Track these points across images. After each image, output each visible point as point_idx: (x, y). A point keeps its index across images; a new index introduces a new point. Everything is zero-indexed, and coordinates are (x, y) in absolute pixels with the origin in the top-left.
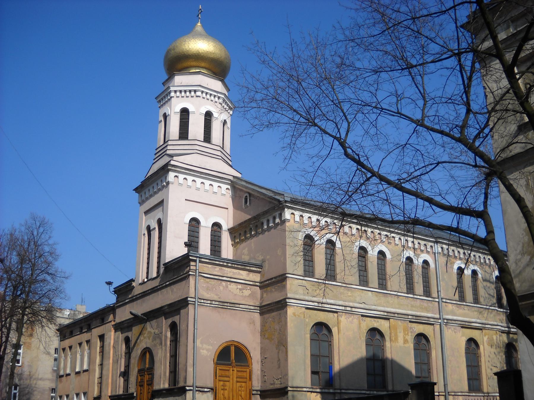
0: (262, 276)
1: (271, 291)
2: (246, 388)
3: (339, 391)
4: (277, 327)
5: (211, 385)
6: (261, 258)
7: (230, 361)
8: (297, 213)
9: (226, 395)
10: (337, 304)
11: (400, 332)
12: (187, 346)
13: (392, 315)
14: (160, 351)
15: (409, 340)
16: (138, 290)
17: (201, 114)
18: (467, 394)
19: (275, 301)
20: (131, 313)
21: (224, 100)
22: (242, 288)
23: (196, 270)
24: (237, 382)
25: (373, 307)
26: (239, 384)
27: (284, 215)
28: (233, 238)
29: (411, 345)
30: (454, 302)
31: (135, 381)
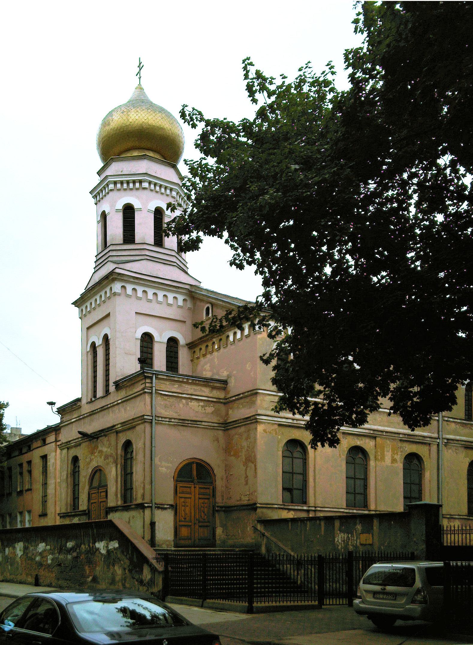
1: (238, 408)
3: (313, 509)
5: (172, 502)
9: (187, 512)
15: (398, 460)
16: (86, 409)
17: (149, 211)
18: (466, 517)
23: (152, 387)
24: (200, 498)
29: (400, 465)
30: (459, 421)
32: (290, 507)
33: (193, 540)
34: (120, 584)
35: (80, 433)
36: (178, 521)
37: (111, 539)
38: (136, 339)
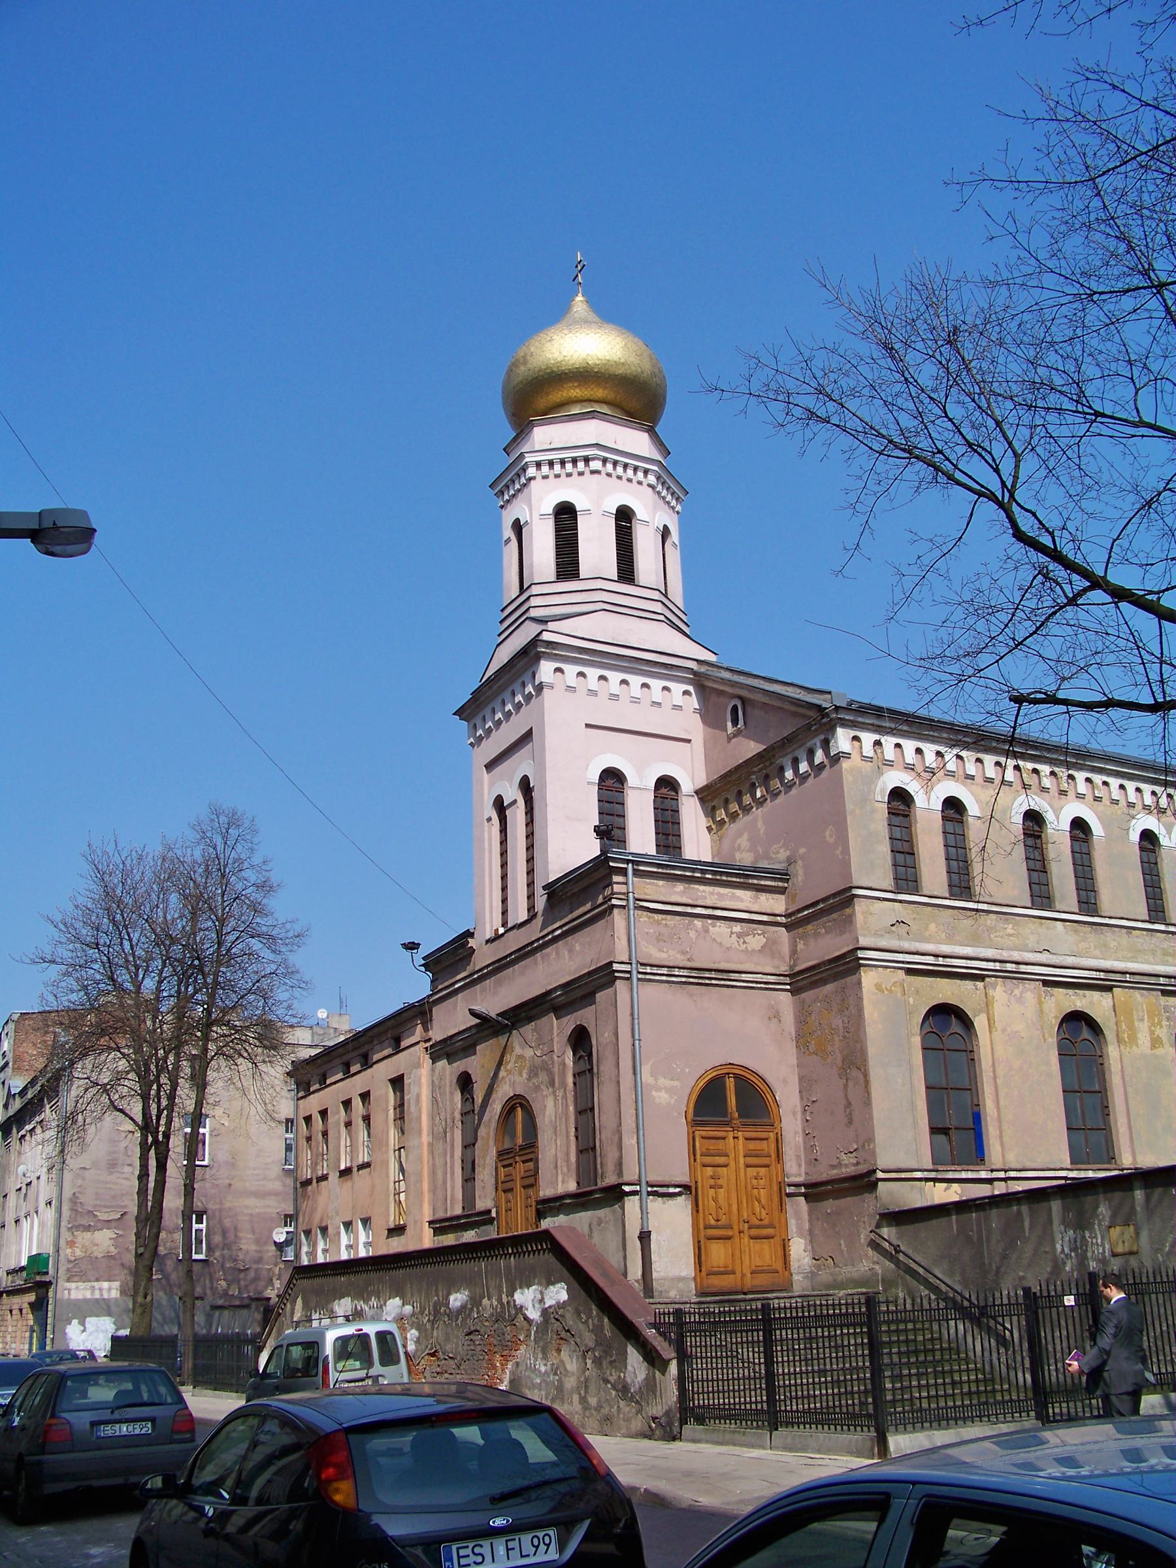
0: (791, 899)
1: (817, 935)
2: (771, 1180)
4: (838, 1022)
5: (685, 1179)
6: (783, 854)
7: (726, 1116)
8: (868, 738)
10: (981, 955)
11: (1142, 1020)
12: (618, 1082)
13: (1118, 977)
14: (550, 1103)
15: (1165, 1039)
16: (483, 957)
17: (606, 513)
19: (827, 958)
20: (473, 1013)
21: (658, 478)
22: (740, 933)
24: (747, 1166)
25: (1070, 961)
26: (752, 1171)
27: (836, 742)
28: (710, 812)
31: (493, 1180)
32: (950, 1175)
33: (739, 1274)
34: (576, 1397)
36: (702, 1226)
37: (550, 1282)
38: (589, 783)
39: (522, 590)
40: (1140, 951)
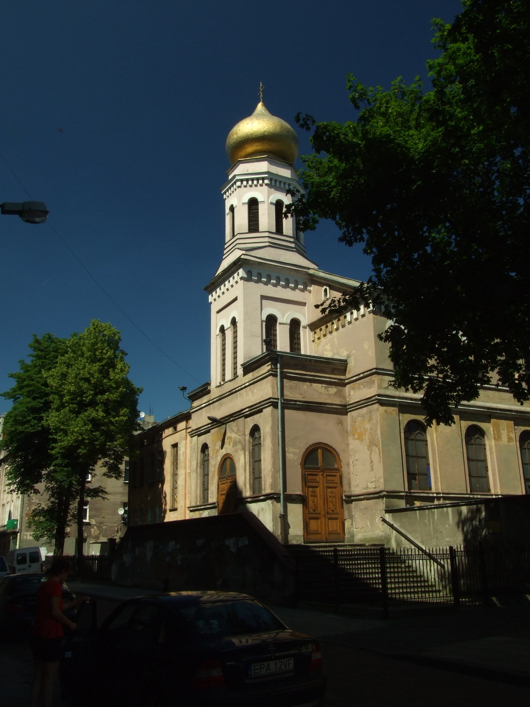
1: (359, 388)
11: (504, 429)
17: (271, 203)
24: (328, 487)
31: (216, 490)
35: (209, 418)
39: (234, 236)
40: (503, 399)
